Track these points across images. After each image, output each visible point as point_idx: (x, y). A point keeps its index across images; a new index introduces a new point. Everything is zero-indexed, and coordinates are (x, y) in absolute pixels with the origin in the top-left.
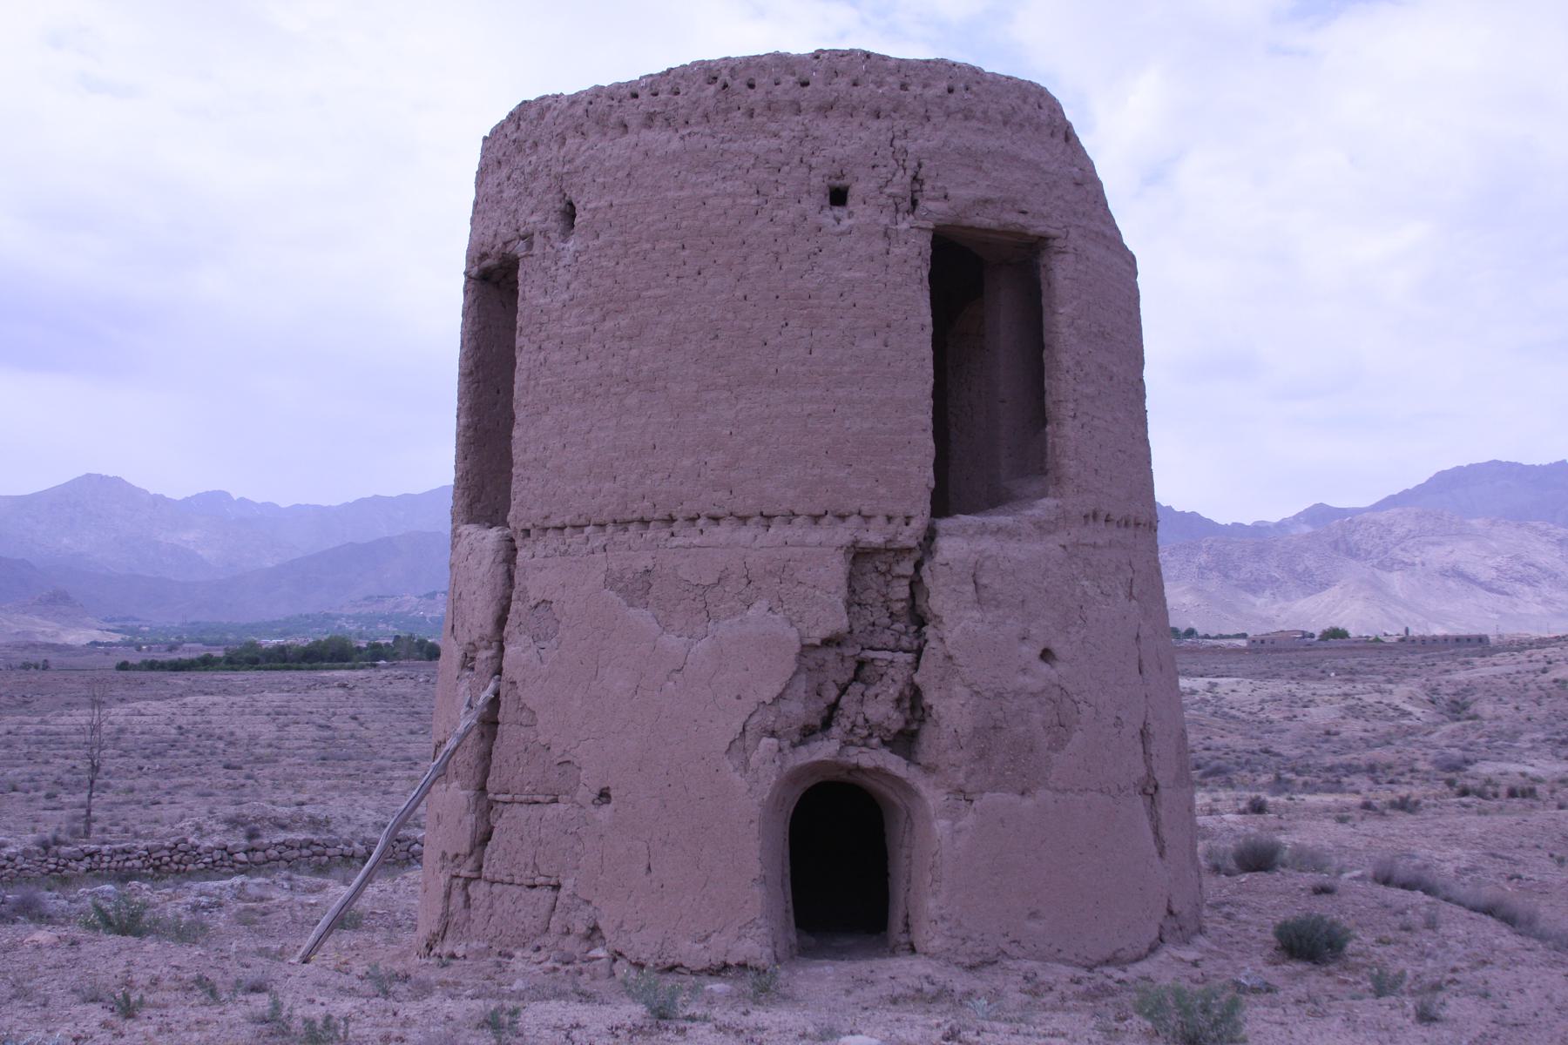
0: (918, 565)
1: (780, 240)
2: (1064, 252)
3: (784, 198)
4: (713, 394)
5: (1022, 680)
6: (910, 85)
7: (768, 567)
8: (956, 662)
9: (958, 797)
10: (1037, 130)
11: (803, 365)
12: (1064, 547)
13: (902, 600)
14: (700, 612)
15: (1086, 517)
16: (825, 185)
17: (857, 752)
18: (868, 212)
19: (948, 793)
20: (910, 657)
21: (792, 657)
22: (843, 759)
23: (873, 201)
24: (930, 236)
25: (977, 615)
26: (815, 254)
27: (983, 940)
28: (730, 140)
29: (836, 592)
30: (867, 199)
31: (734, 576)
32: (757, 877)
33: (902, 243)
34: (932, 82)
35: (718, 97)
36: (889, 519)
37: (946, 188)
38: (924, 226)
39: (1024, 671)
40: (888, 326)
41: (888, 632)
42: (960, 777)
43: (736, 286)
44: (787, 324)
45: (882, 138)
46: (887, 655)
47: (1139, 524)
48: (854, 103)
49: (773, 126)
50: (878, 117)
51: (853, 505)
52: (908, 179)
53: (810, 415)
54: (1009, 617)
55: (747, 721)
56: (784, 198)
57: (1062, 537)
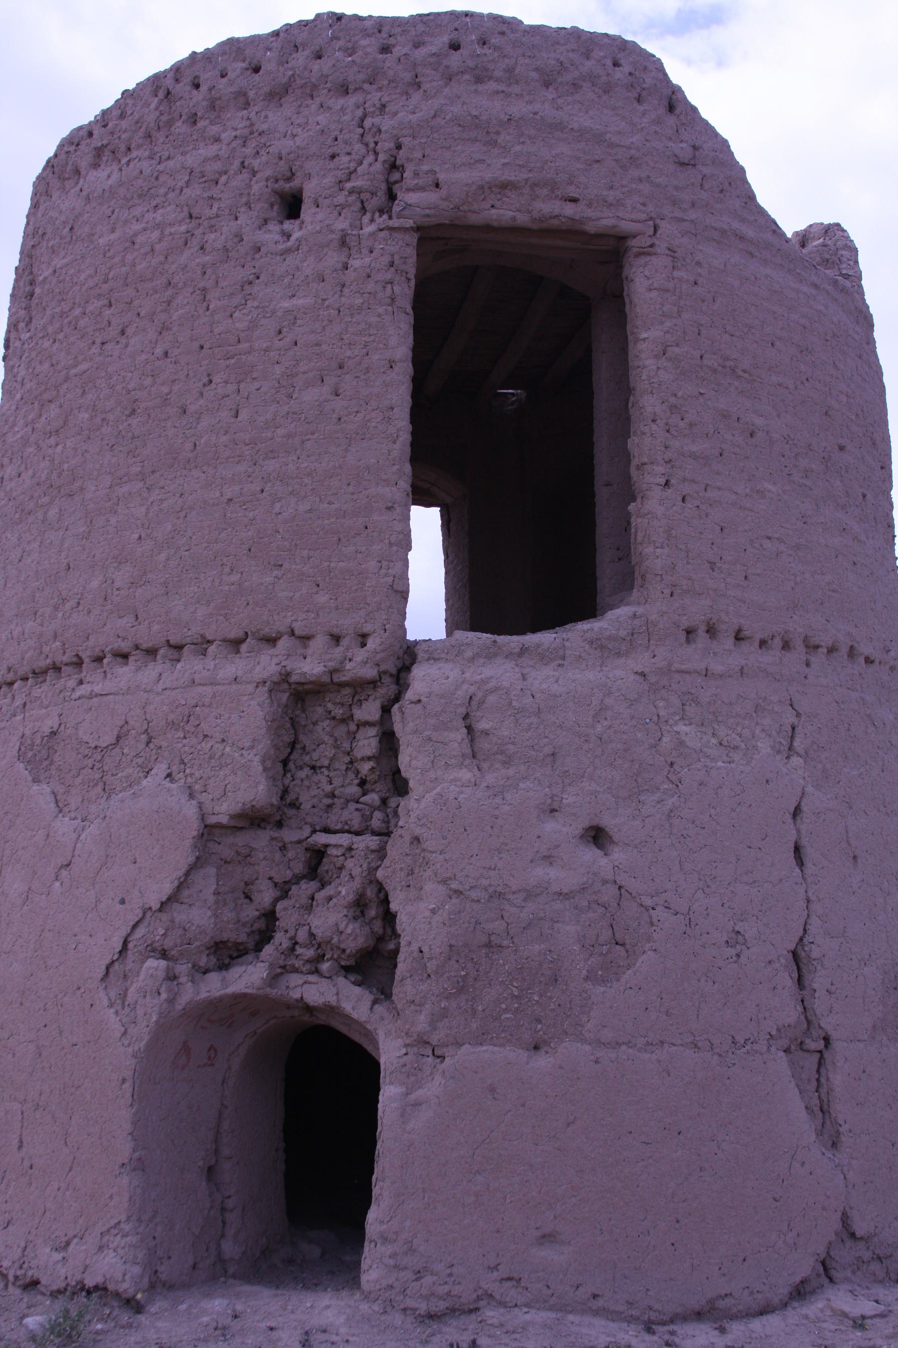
0: (386, 710)
1: (209, 272)
2: (649, 254)
3: (218, 216)
4: (125, 489)
5: (540, 872)
6: (394, 46)
7: (171, 717)
8: (425, 846)
9: (422, 1051)
10: (606, 92)
11: (226, 432)
12: (643, 675)
13: (369, 759)
14: (96, 785)
15: (689, 632)
16: (269, 190)
17: (301, 982)
18: (320, 216)
19: (406, 1046)
20: (372, 842)
21: (188, 842)
22: (274, 992)
23: (327, 201)
24: (413, 238)
25: (466, 775)
26: (251, 283)
27: (451, 1275)
28: (169, 158)
29: (252, 747)
30: (320, 200)
31: (133, 732)
32: (126, 1161)
33: (365, 251)
34: (426, 39)
35: (161, 108)
36: (336, 639)
37: (435, 172)
38: (396, 225)
39: (548, 859)
40: (341, 367)
41: (352, 806)
42: (422, 1022)
43: (156, 342)
44: (211, 382)
45: (346, 118)
46: (344, 839)
47: (817, 647)
48: (313, 80)
49: (215, 129)
50: (348, 93)
51: (280, 624)
52: (378, 166)
53: (230, 500)
54: (525, 778)
55: (129, 935)
56: (218, 216)
57: (641, 661)
